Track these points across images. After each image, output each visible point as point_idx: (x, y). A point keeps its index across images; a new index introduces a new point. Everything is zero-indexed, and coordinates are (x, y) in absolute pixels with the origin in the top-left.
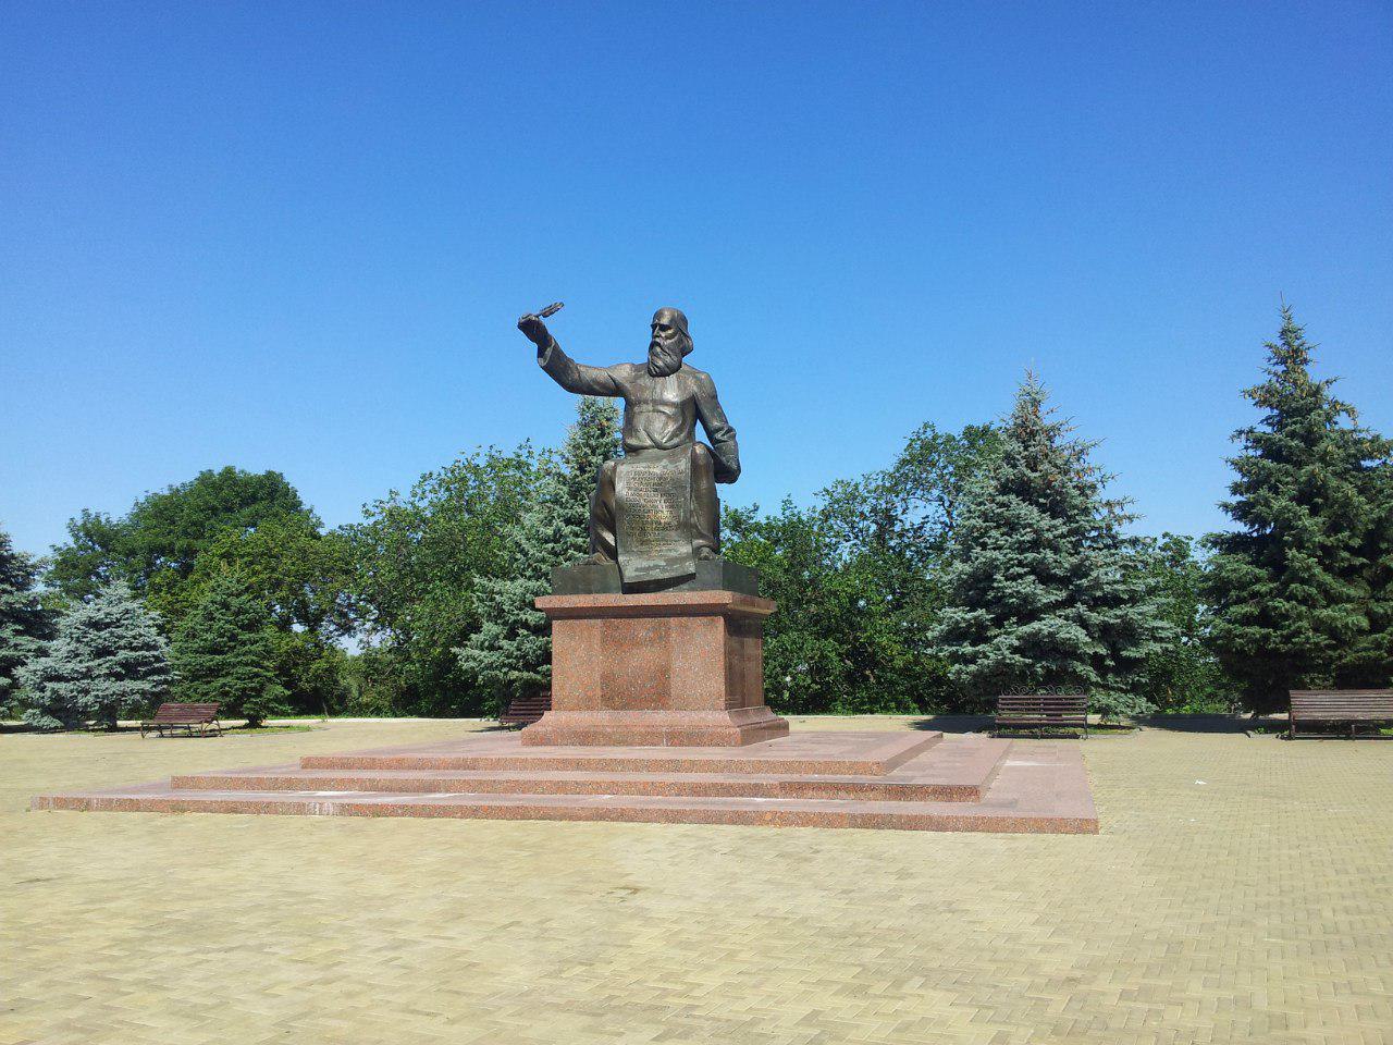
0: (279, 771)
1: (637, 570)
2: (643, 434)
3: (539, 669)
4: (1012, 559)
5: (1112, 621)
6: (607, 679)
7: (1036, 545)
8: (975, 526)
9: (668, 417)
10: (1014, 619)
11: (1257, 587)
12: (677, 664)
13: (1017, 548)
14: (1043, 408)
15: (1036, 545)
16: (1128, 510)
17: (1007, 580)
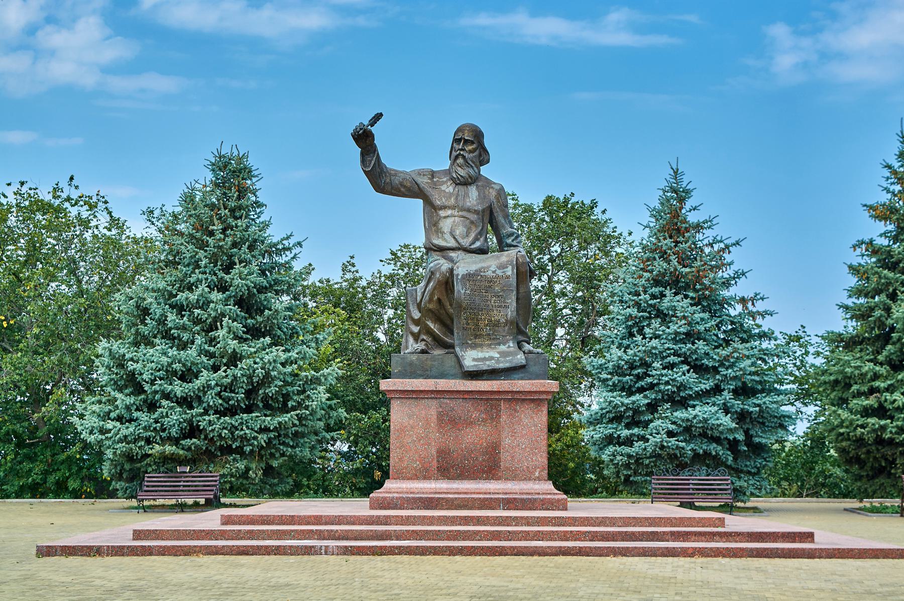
0: (720, 496)
1: (474, 360)
2: (448, 236)
3: (183, 442)
4: (669, 349)
5: (751, 409)
6: (443, 453)
7: (691, 336)
8: (630, 315)
9: (472, 222)
10: (668, 405)
11: (877, 384)
12: (507, 441)
13: (672, 339)
14: (688, 204)
15: (691, 336)
16: (760, 306)
17: (664, 368)
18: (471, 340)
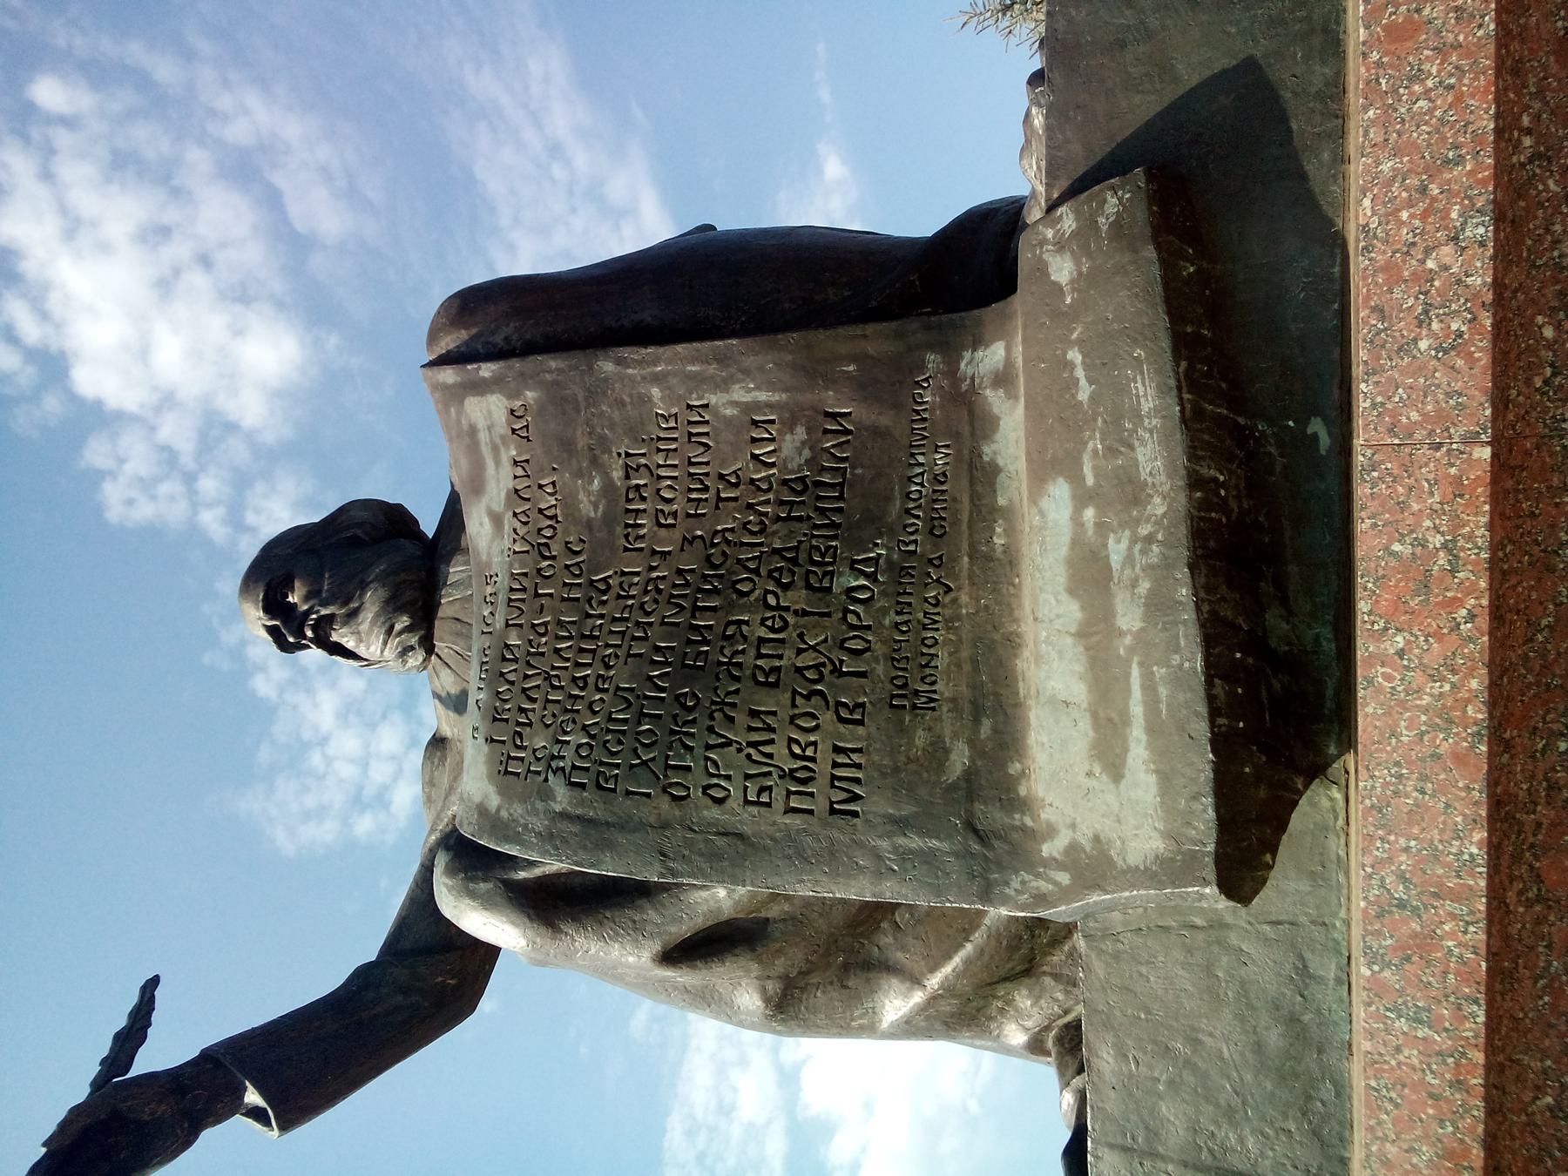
1: (1109, 754)
18: (938, 752)
